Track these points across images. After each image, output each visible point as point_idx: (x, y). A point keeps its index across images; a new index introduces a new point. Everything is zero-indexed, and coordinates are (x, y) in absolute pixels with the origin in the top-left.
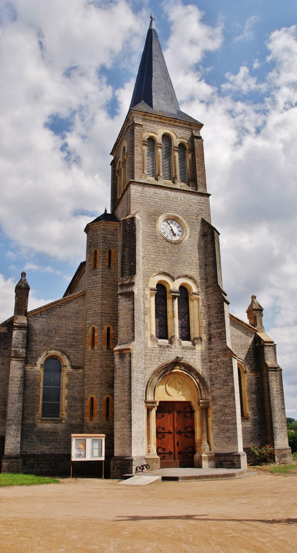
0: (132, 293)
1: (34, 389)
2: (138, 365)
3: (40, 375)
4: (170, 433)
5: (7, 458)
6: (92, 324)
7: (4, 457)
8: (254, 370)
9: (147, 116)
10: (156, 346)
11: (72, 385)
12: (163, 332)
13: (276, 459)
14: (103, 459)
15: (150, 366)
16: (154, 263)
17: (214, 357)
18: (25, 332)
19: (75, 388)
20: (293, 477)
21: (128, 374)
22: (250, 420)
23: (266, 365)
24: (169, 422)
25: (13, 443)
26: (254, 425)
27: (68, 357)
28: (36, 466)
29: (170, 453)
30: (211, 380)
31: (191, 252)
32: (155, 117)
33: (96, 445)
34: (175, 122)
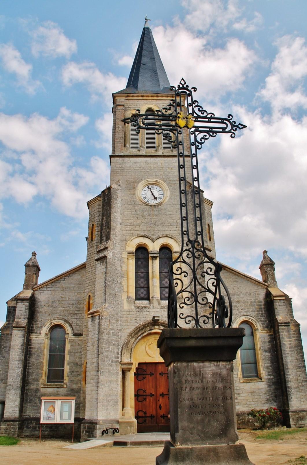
0: (105, 257)
1: (39, 356)
2: (111, 327)
3: (44, 343)
4: (152, 395)
5: (5, 421)
6: (89, 292)
7: (3, 420)
8: (267, 327)
9: (129, 96)
10: (133, 307)
11: (74, 351)
12: (143, 293)
13: (292, 423)
14: (72, 421)
15: (126, 327)
16: (132, 227)
18: (27, 304)
19: (76, 354)
20: (260, 445)
21: (97, 336)
22: (263, 380)
23: (277, 321)
24: (151, 384)
25: (12, 407)
26: (269, 386)
27: (71, 325)
28: (38, 429)
29: (152, 417)
31: (171, 213)
32: (137, 96)
33: (66, 408)
34: (158, 96)
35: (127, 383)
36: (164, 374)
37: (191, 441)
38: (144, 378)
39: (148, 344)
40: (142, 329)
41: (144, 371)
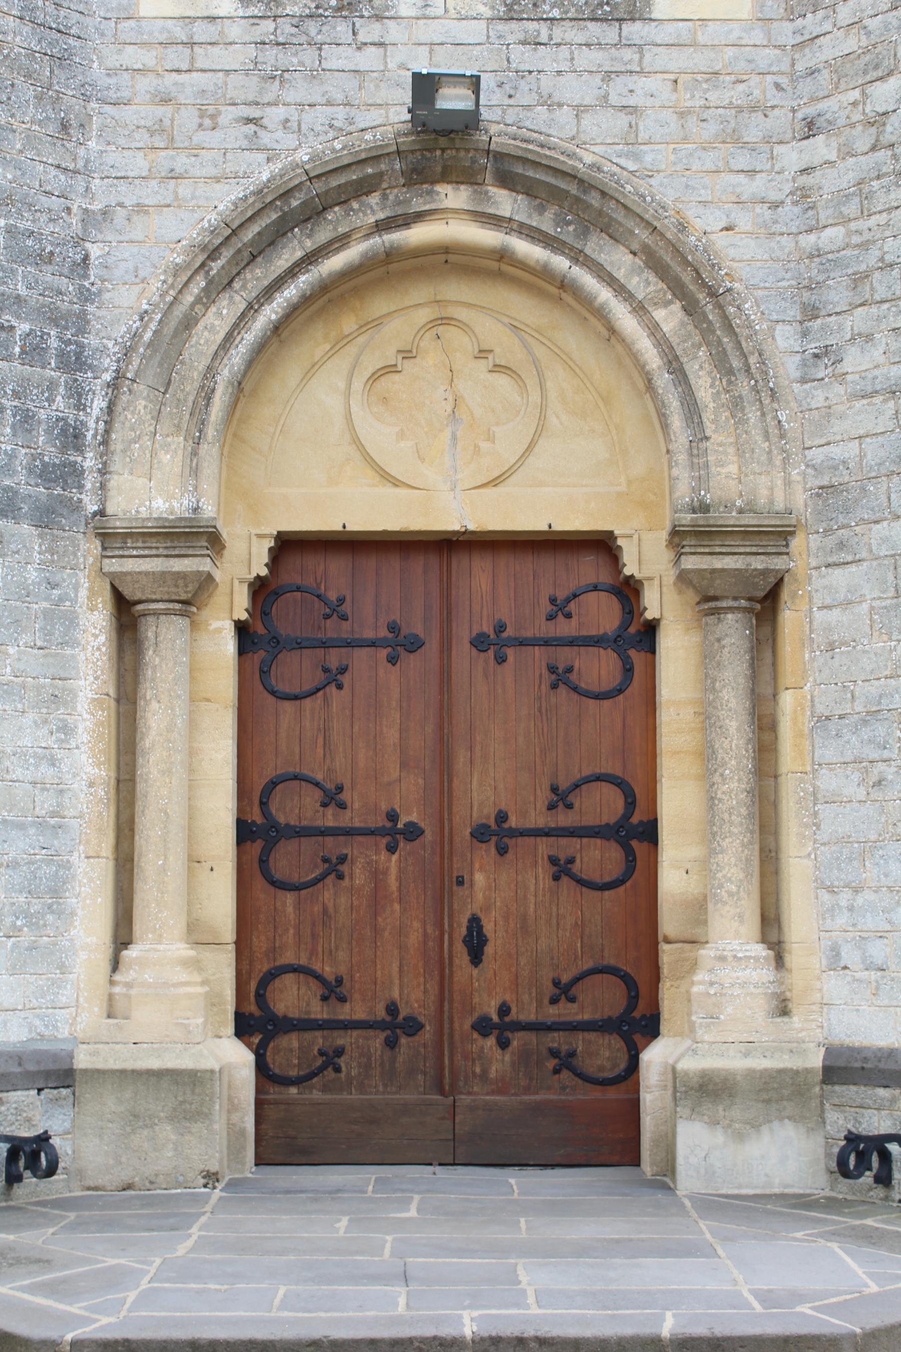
4: (395, 833)
15: (150, 194)
17: (839, 68)
29: (396, 1025)
30: (811, 312)
35: (158, 717)
36: (522, 643)
37: (705, 637)
38: (334, 678)
39: (371, 363)
40: (312, 214)
41: (336, 610)
